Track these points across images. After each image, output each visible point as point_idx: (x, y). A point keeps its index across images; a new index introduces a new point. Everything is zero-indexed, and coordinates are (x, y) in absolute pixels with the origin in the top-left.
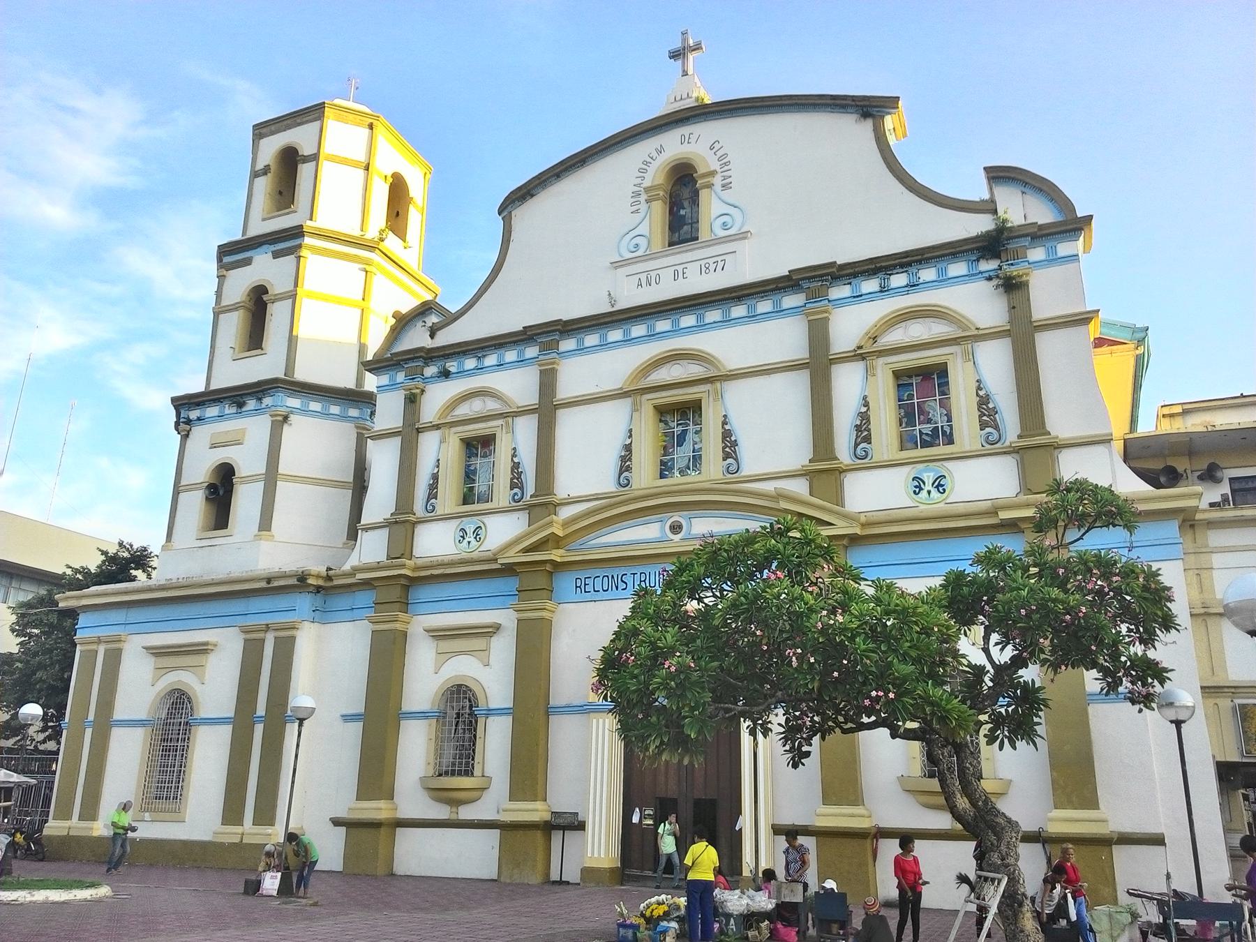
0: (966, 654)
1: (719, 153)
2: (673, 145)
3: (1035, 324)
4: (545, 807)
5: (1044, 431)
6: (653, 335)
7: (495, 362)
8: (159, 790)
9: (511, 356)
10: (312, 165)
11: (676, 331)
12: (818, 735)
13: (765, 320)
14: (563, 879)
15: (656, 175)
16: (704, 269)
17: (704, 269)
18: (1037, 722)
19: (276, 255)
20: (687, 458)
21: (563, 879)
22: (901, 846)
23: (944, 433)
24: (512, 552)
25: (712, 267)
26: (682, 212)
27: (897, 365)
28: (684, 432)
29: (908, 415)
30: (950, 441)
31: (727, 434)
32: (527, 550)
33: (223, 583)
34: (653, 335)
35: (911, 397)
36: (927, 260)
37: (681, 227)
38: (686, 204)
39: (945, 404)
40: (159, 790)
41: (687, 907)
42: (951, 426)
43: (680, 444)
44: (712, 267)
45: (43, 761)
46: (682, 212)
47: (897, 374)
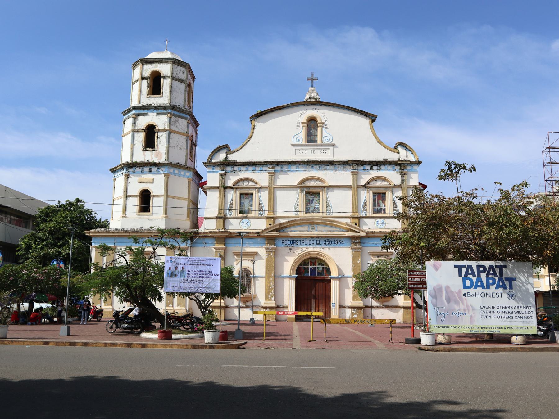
0: (498, 406)
1: (325, 117)
2: (310, 112)
4: (185, 309)
10: (452, 338)
12: (200, 189)
15: (304, 120)
16: (320, 152)
17: (320, 152)
20: (313, 208)
23: (383, 210)
25: (323, 152)
26: (311, 131)
28: (313, 200)
29: (375, 204)
30: (384, 212)
31: (328, 204)
35: (375, 199)
37: (311, 136)
38: (312, 129)
39: (384, 202)
41: (47, 319)
42: (385, 208)
43: (312, 203)
44: (323, 152)
46: (311, 131)
47: (373, 193)
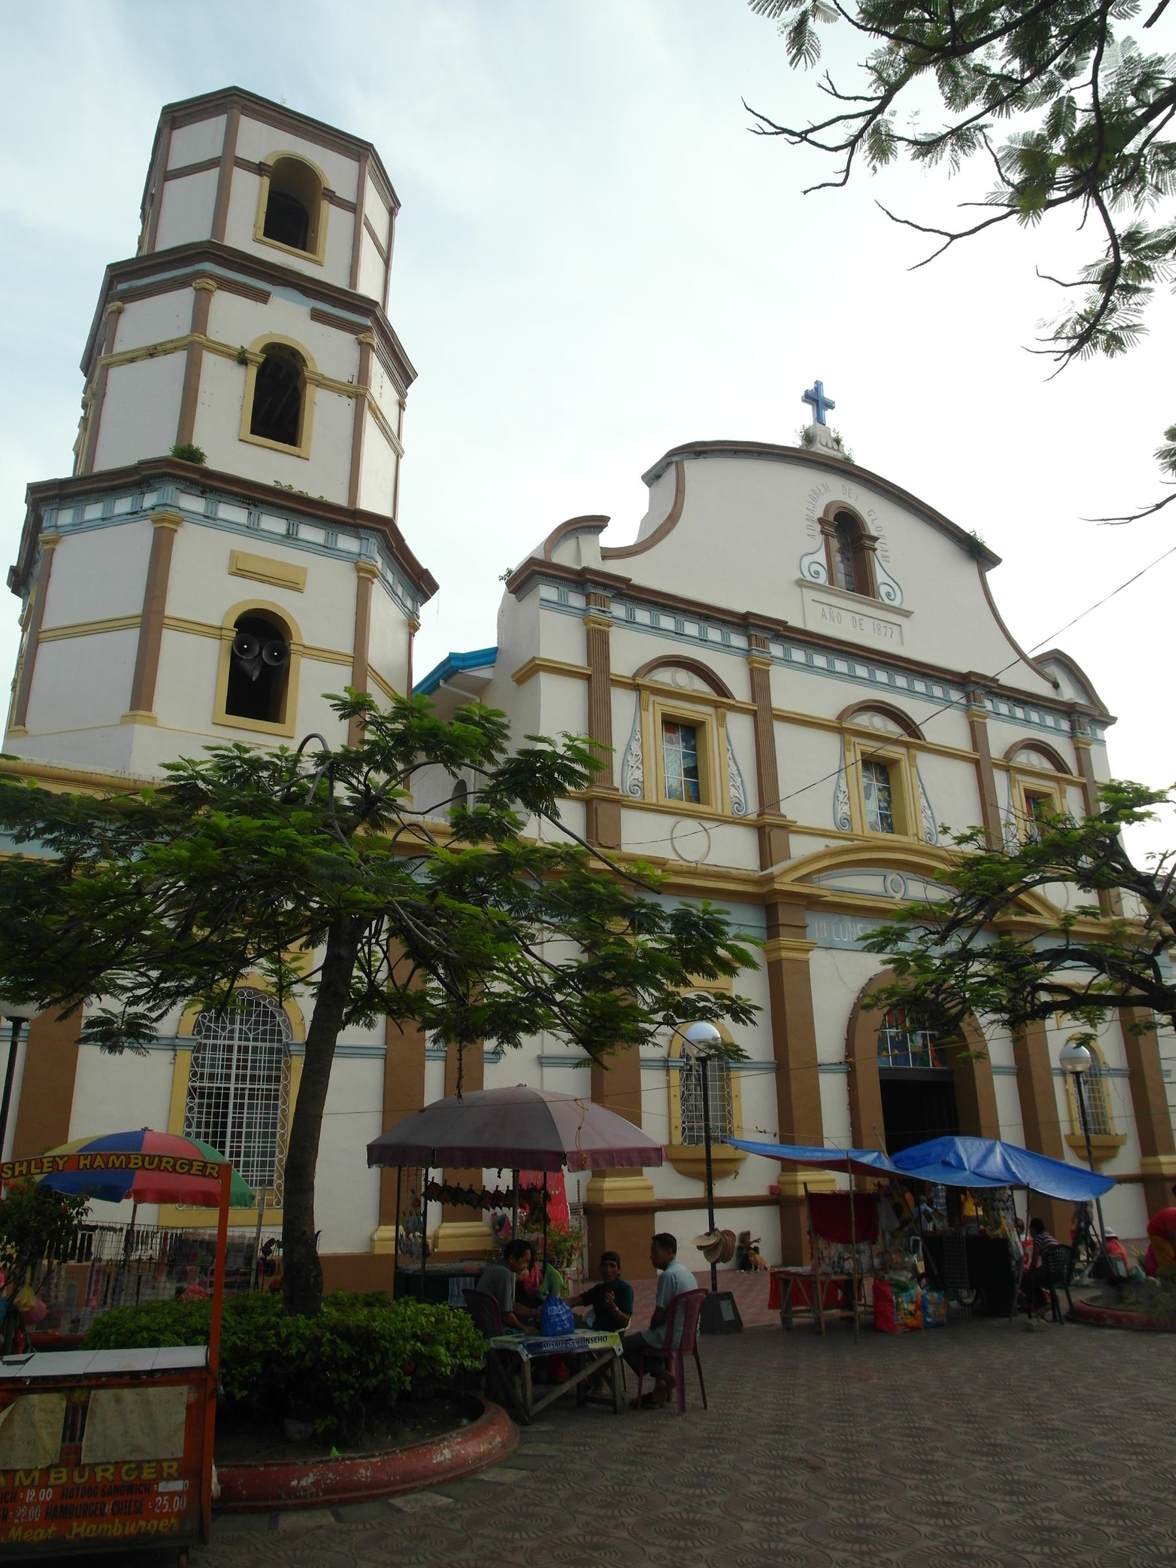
3: (612, 677)
5: (777, 813)
6: (831, 672)
7: (128, 509)
8: (252, 1145)
9: (123, 505)
11: (891, 687)
13: (817, 673)
14: (706, 1212)
18: (706, 1065)
19: (317, 316)
21: (706, 1212)
22: (118, 1200)
24: (788, 879)
27: (670, 709)
32: (800, 879)
33: (719, 877)
34: (831, 672)
36: (356, 527)
40: (252, 1145)
45: (210, 1096)
